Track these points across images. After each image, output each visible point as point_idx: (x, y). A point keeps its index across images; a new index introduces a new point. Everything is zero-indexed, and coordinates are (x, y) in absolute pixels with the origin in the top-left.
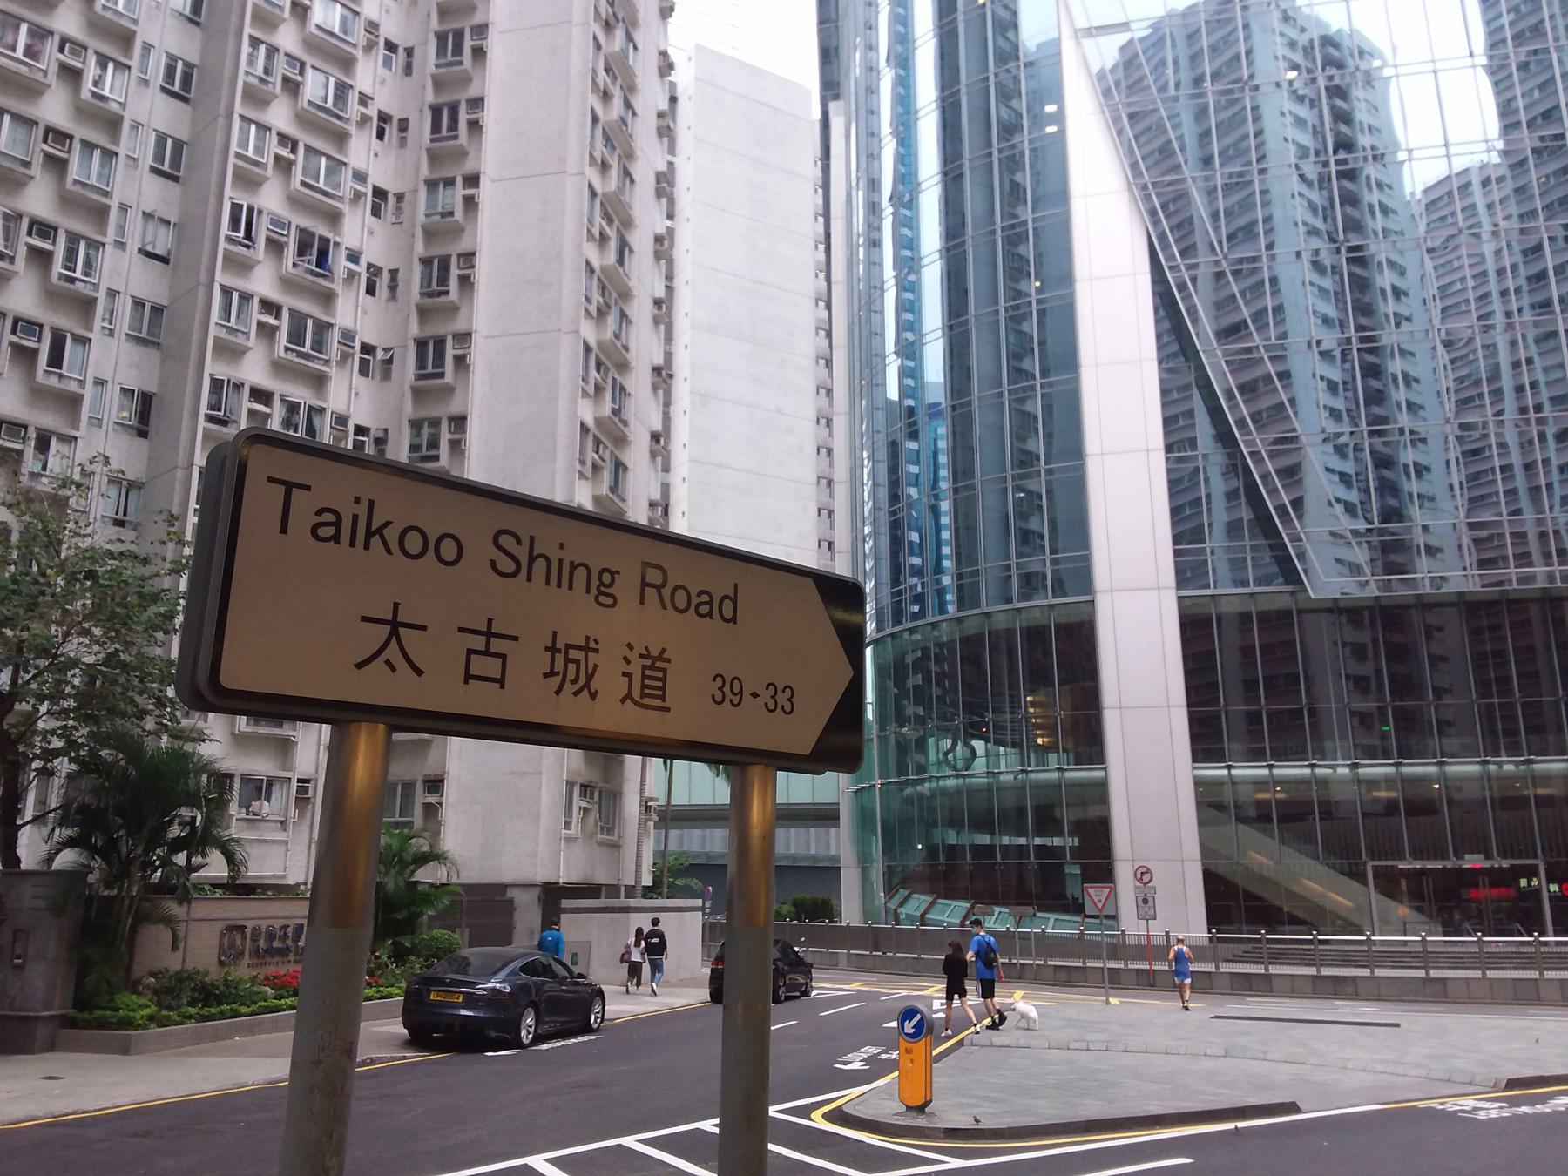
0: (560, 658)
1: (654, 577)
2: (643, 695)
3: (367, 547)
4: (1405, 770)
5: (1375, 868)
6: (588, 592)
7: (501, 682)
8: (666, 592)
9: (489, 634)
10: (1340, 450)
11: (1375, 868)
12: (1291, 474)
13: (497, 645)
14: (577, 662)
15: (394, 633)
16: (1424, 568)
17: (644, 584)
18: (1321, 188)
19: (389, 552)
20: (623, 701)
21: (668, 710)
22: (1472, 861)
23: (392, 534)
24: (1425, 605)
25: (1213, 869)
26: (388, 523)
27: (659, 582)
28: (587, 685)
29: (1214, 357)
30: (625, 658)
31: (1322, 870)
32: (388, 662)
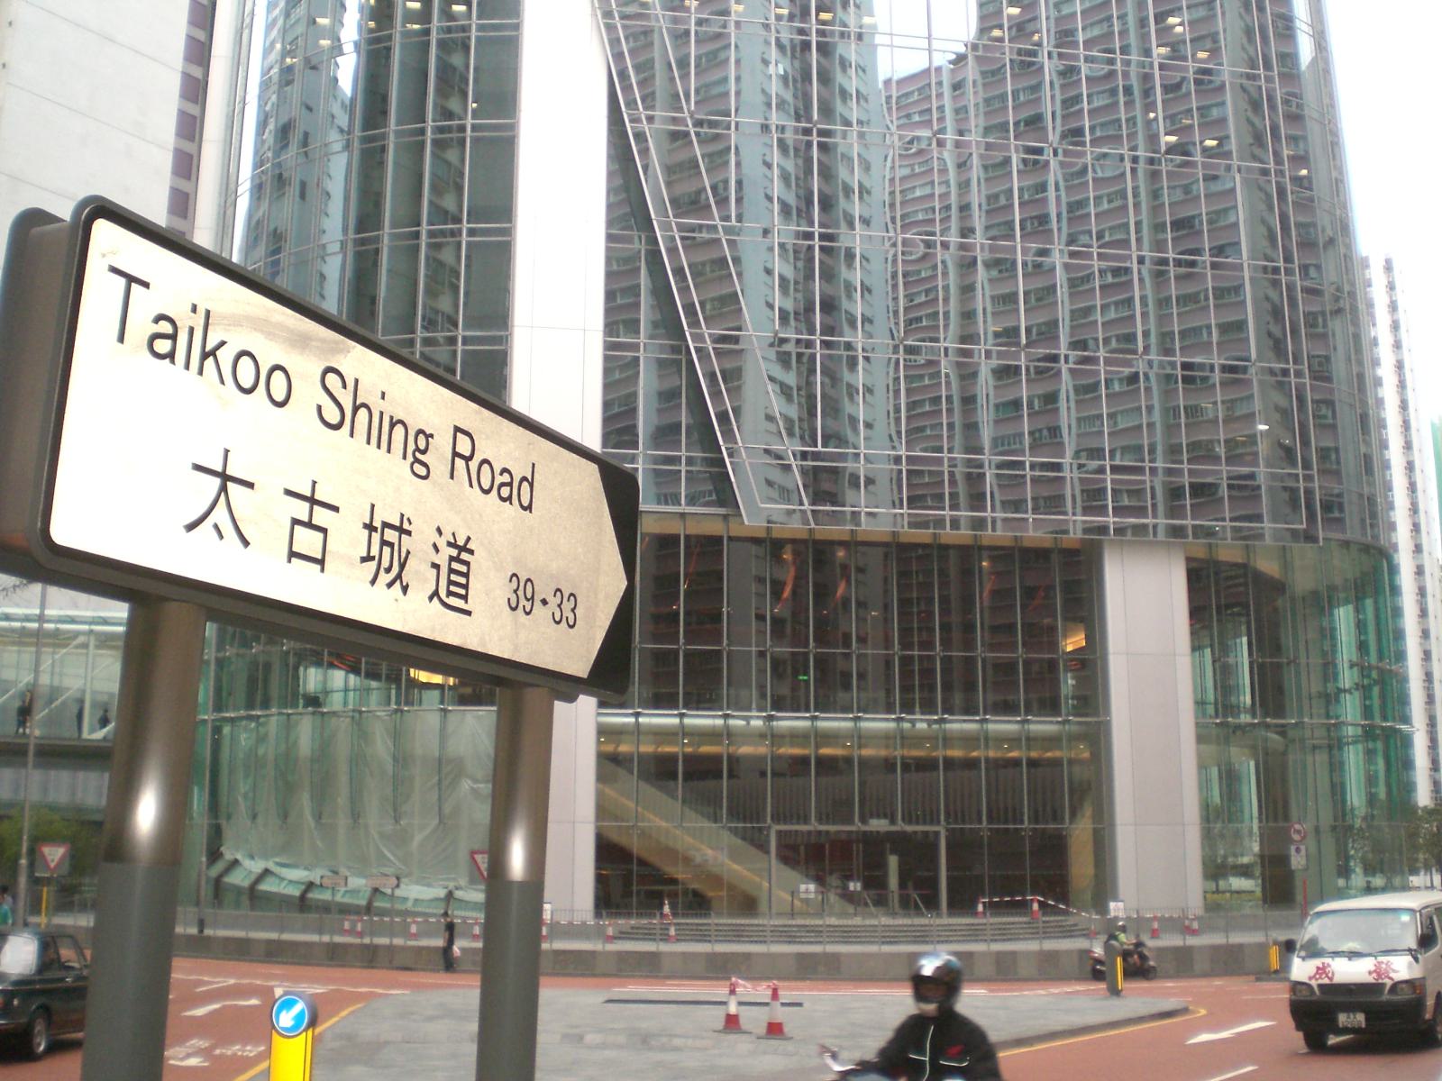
0: (376, 537)
1: (464, 446)
2: (450, 593)
3: (201, 372)
4: (820, 724)
5: (779, 833)
6: (405, 457)
7: (321, 562)
8: (474, 465)
9: (312, 501)
10: (784, 359)
11: (779, 833)
12: (733, 376)
13: (321, 516)
14: (391, 545)
15: (224, 489)
16: (860, 501)
17: (455, 454)
18: (793, 57)
19: (222, 382)
20: (431, 599)
21: (468, 613)
22: (878, 825)
23: (225, 356)
24: (853, 544)
25: (615, 837)
26: (223, 343)
27: (467, 454)
28: (399, 576)
29: (666, 227)
30: (435, 546)
31: (727, 838)
32: (216, 527)
